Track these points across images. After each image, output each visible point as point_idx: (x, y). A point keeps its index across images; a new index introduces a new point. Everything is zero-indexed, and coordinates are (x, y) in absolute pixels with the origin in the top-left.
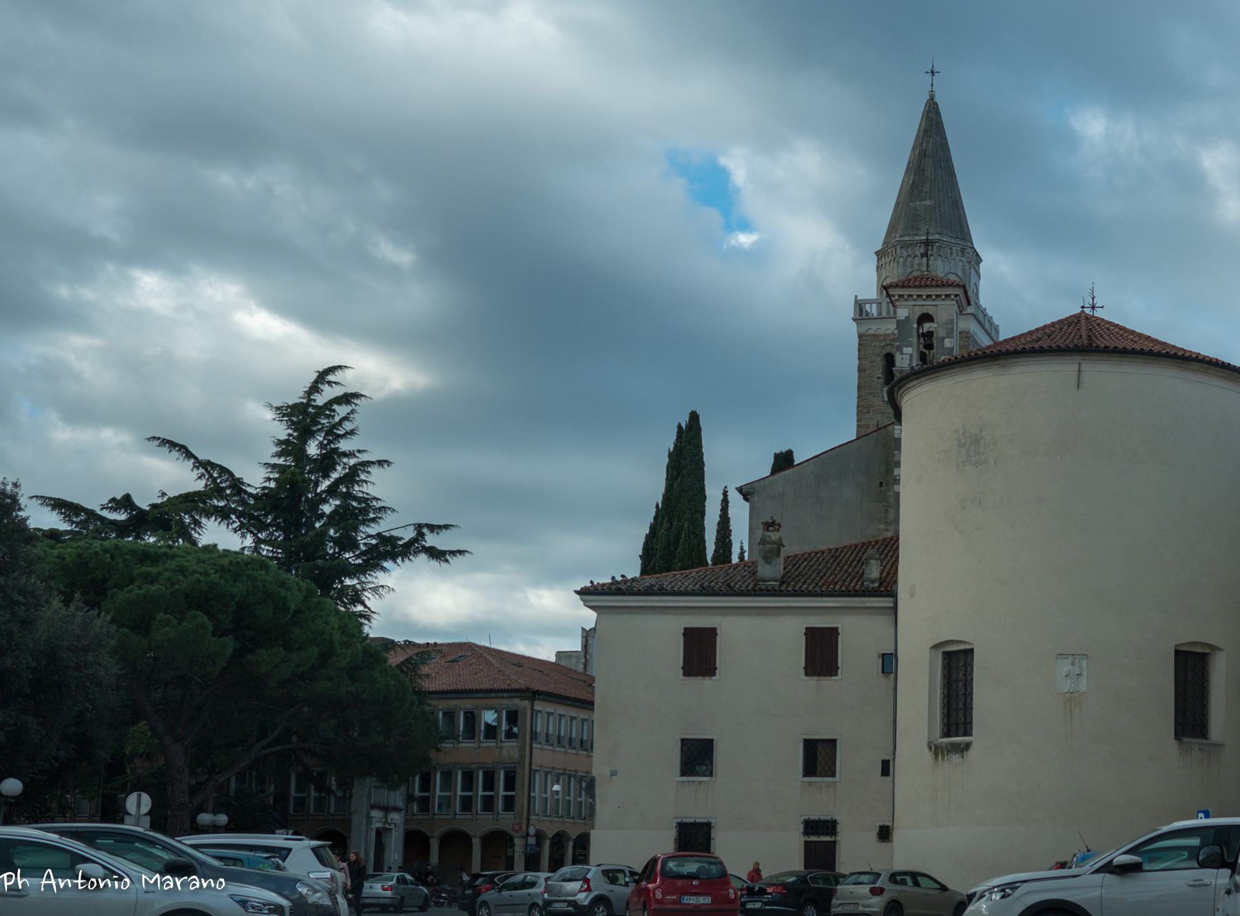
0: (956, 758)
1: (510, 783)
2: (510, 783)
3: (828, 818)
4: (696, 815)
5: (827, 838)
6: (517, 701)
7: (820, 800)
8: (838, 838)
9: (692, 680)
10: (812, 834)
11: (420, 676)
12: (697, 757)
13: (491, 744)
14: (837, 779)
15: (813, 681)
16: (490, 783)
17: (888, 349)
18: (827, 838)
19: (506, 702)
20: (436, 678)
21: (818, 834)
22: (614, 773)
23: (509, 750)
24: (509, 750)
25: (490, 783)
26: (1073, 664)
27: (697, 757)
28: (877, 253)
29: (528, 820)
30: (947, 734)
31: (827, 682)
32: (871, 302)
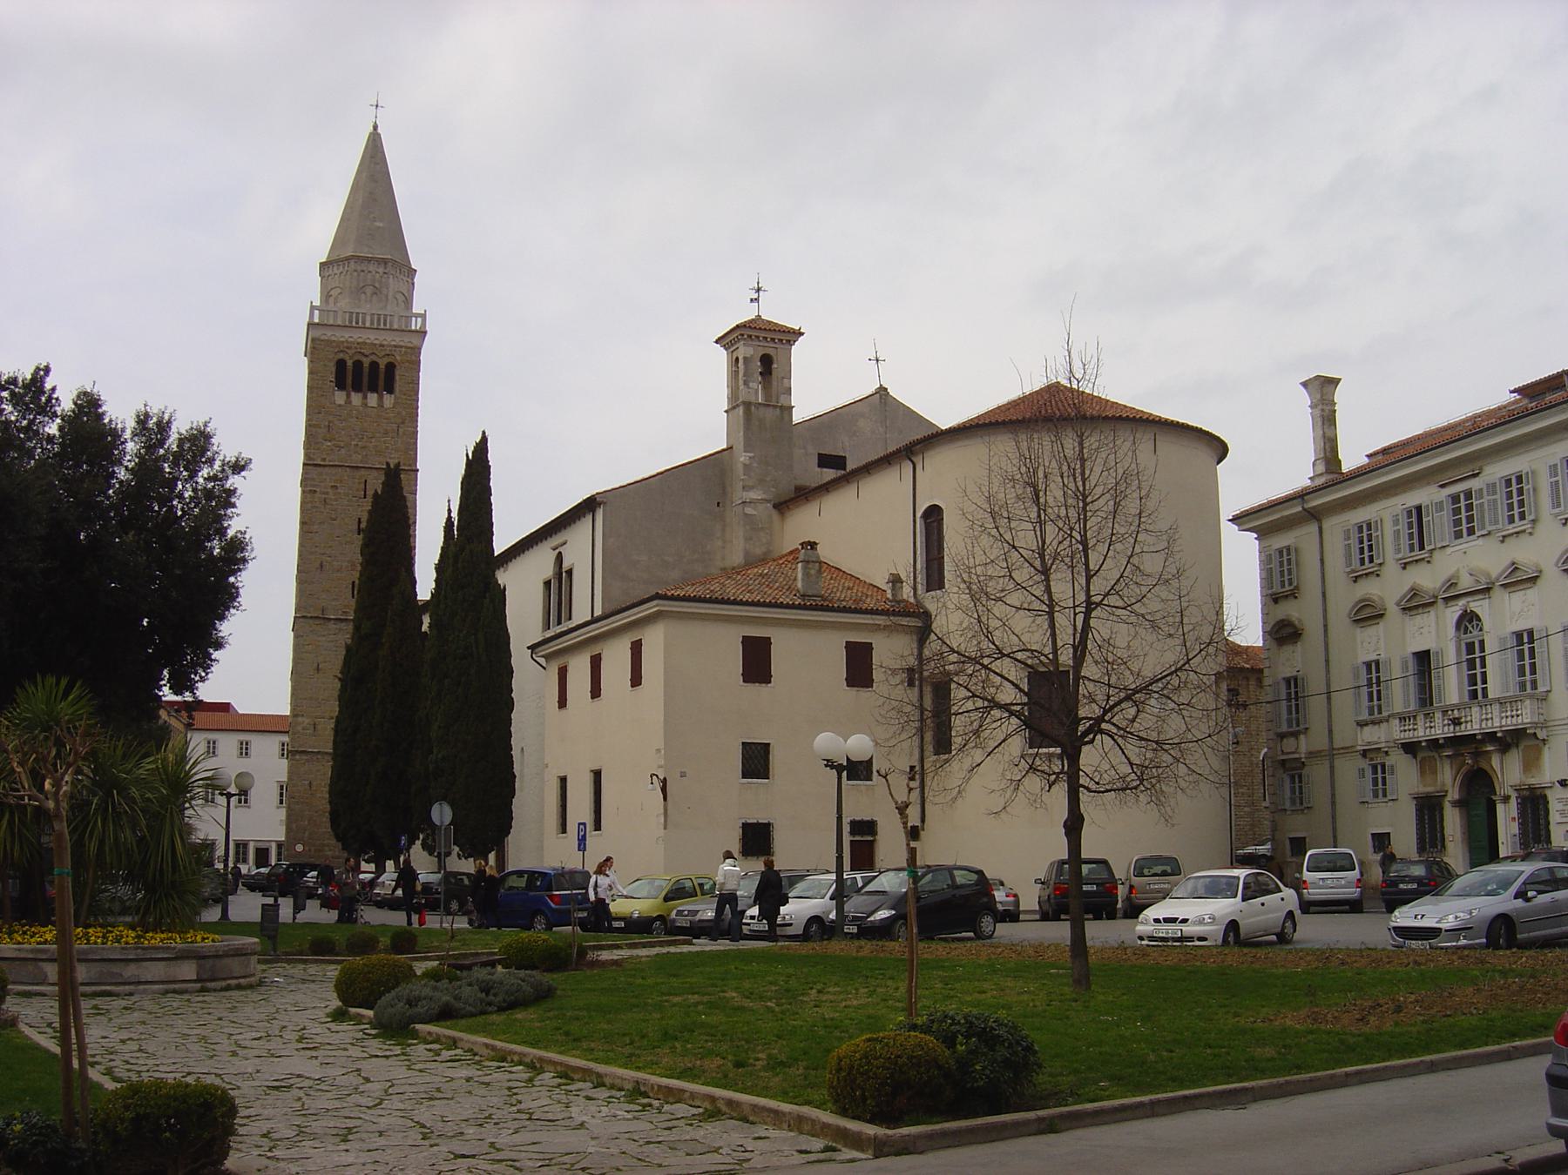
15: (853, 691)
17: (341, 356)
21: (862, 834)
27: (756, 761)
28: (322, 265)
31: (864, 694)
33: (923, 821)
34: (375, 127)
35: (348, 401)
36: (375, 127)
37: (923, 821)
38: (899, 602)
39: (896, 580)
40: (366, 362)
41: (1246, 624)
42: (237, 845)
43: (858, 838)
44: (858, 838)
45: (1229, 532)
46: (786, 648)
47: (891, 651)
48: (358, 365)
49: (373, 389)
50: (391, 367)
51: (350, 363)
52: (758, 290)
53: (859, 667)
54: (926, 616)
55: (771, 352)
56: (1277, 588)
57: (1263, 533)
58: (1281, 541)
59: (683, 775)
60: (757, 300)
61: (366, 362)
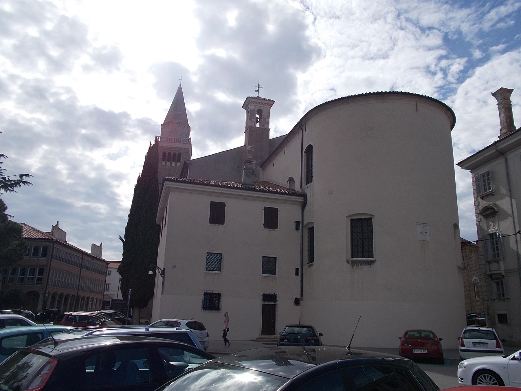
0: (366, 268)
1: (41, 272)
2: (41, 272)
3: (273, 293)
4: (269, 291)
5: (273, 303)
6: (48, 243)
7: (270, 285)
8: (277, 303)
9: (213, 226)
10: (266, 301)
11: (257, 132)
12: (215, 262)
13: (35, 258)
14: (277, 275)
15: (267, 230)
16: (33, 271)
18: (273, 303)
19: (43, 243)
20: (474, 70)
21: (268, 301)
22: (174, 267)
23: (42, 260)
24: (42, 260)
25: (33, 271)
26: (423, 228)
27: (215, 262)
29: (46, 287)
30: (352, 258)
31: (273, 231)
32: (159, 137)
33: (302, 295)
34: (180, 86)
35: (166, 164)
36: (180, 86)
37: (302, 295)
38: (292, 190)
39: (291, 180)
40: (172, 153)
41: (468, 228)
42: (470, 322)
43: (266, 303)
44: (266, 303)
45: (457, 169)
46: (234, 208)
47: (288, 214)
48: (169, 153)
49: (174, 161)
50: (180, 154)
51: (167, 153)
52: (259, 87)
53: (271, 219)
54: (305, 196)
55: (262, 108)
56: (483, 193)
57: (472, 169)
58: (483, 170)
59: (174, 267)
60: (258, 91)
61: (172, 153)
